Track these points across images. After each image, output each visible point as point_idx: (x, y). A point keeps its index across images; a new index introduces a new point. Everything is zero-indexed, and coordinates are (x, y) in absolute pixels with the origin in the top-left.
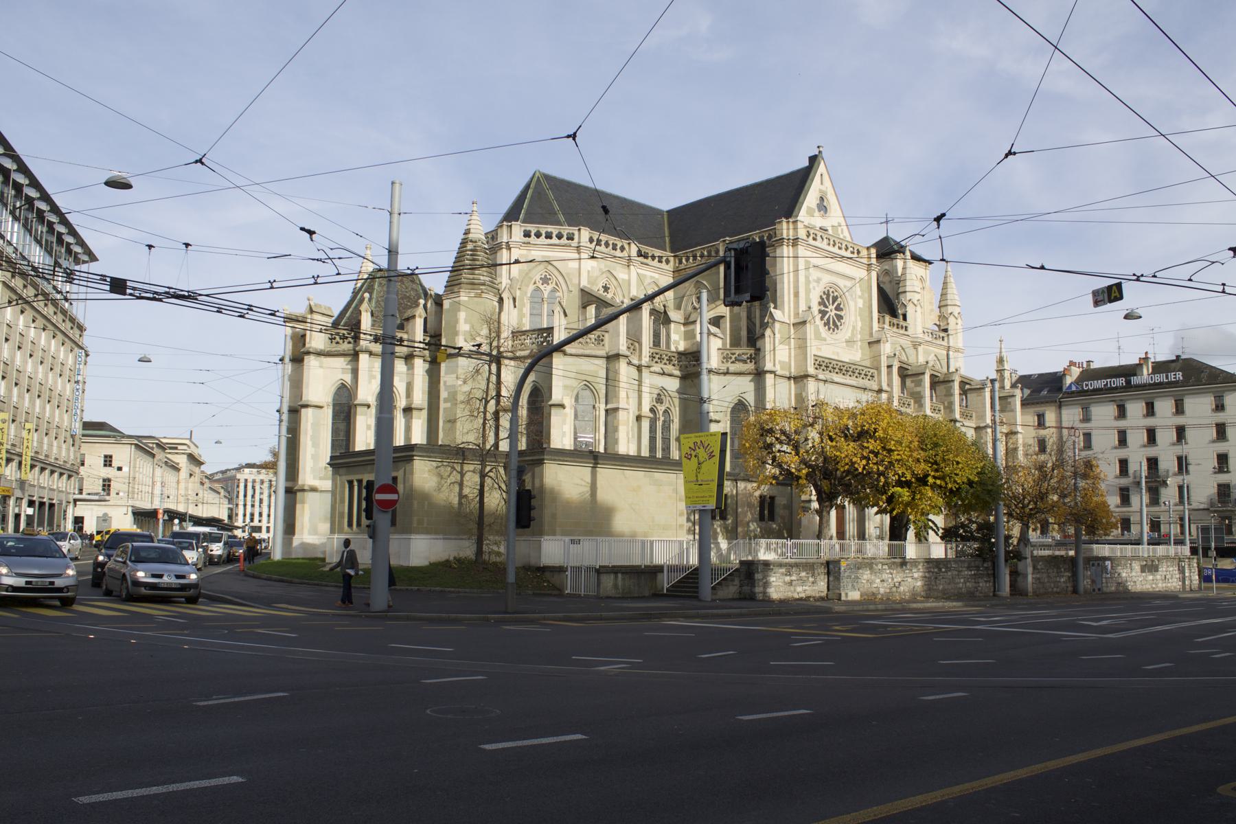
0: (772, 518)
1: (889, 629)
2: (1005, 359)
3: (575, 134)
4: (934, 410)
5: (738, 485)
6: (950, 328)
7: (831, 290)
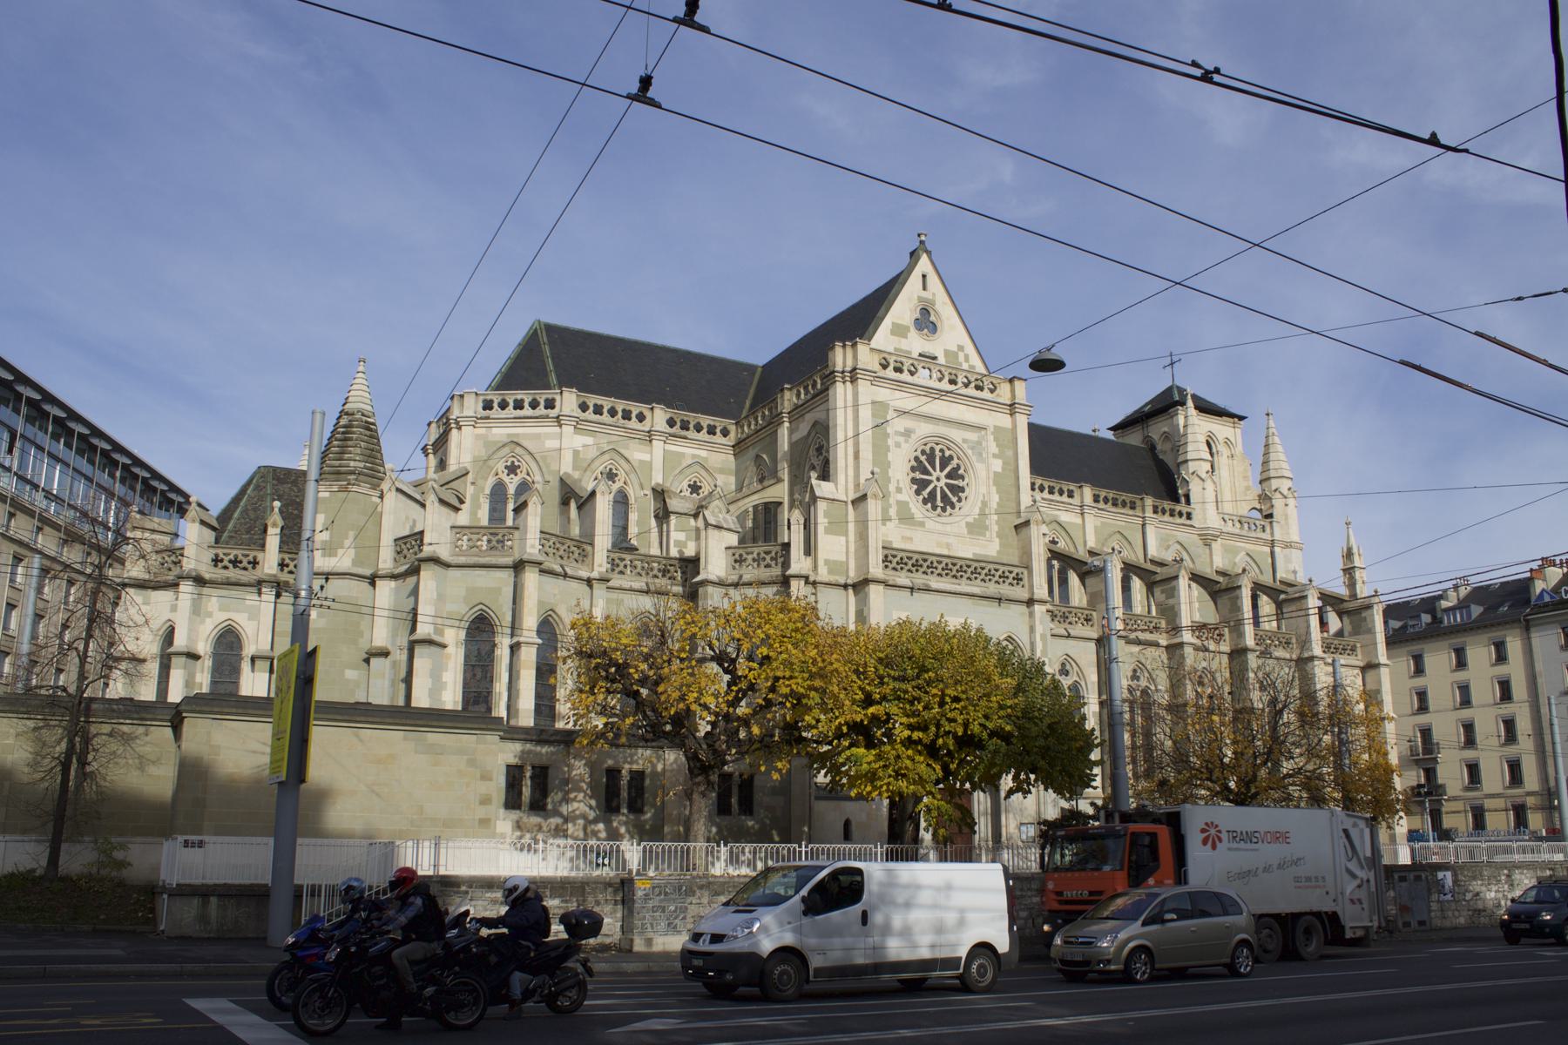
0: (747, 807)
2: (1355, 550)
5: (666, 756)
6: (1276, 512)
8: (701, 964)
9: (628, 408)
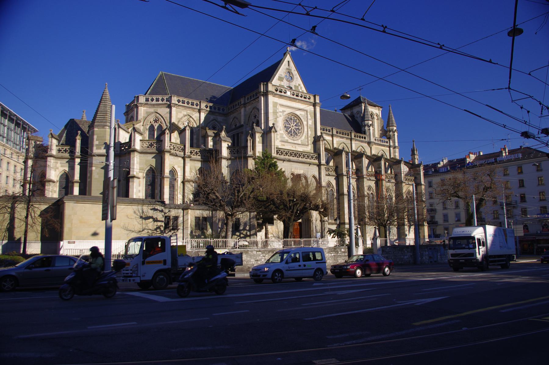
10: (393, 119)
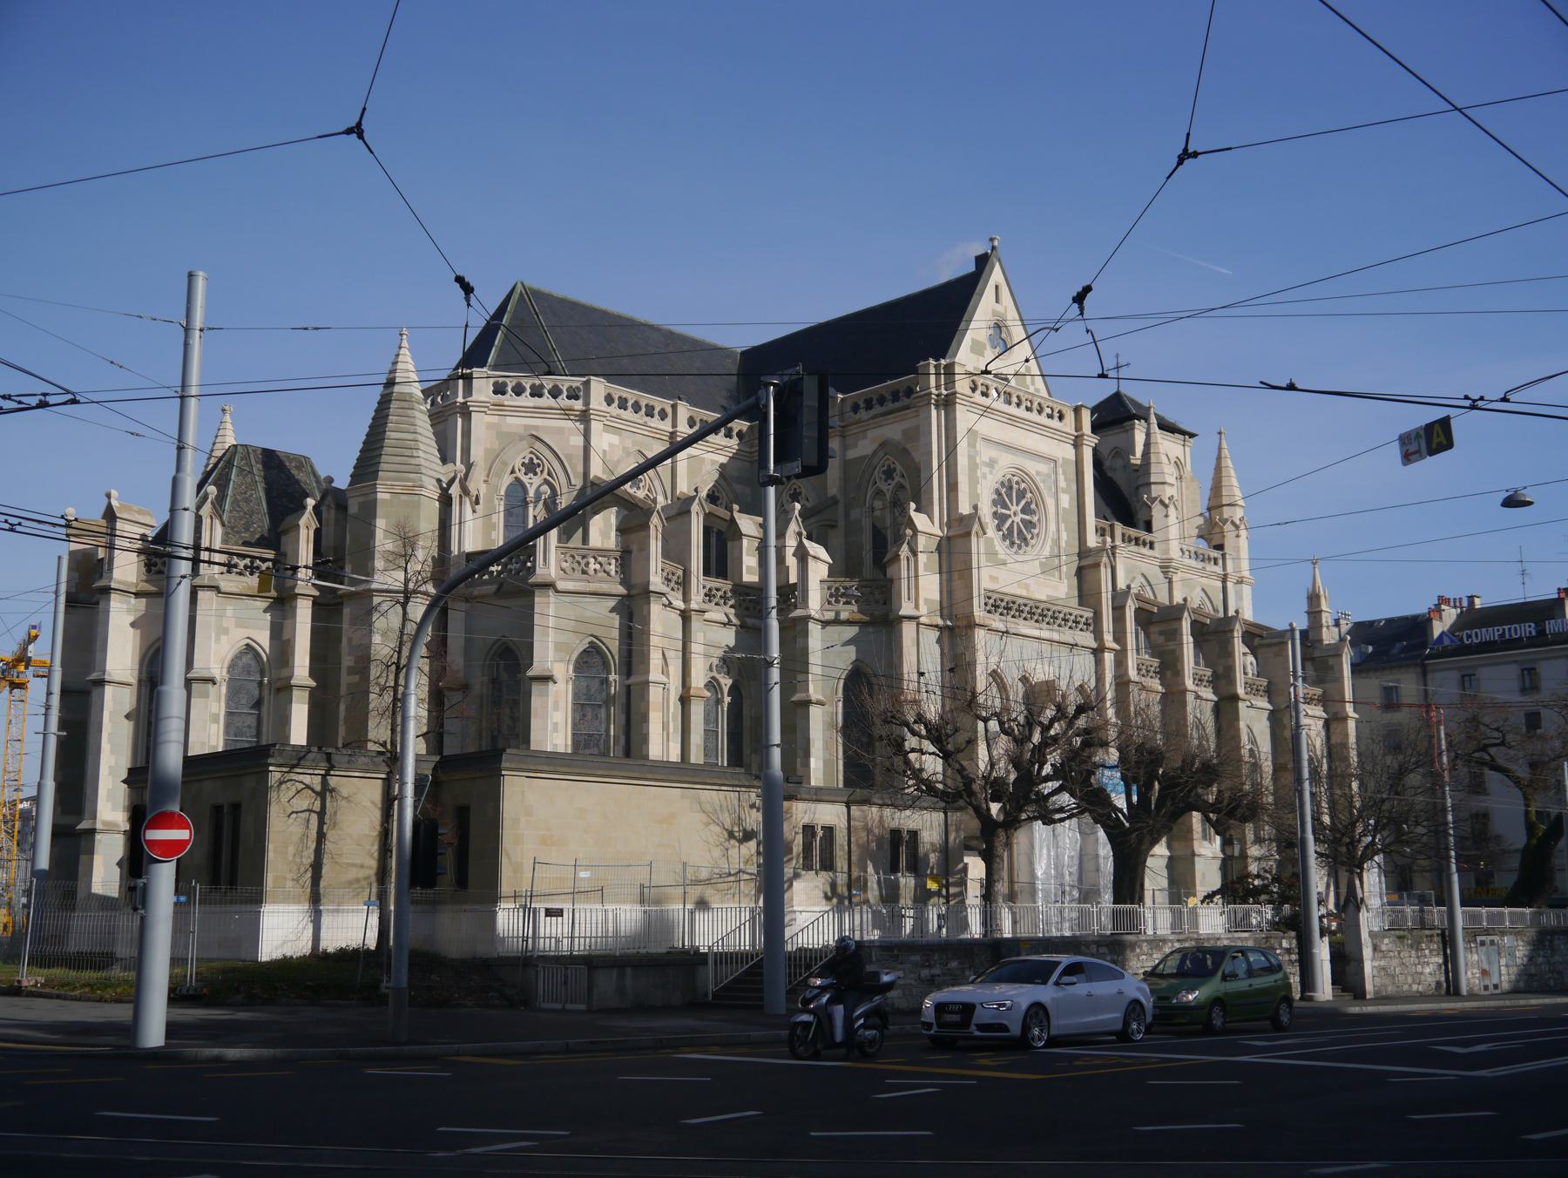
1: (1077, 1063)
3: (359, 124)
4: (1200, 680)
7: (1016, 479)
8: (959, 1019)
9: (651, 403)
10: (1235, 482)
